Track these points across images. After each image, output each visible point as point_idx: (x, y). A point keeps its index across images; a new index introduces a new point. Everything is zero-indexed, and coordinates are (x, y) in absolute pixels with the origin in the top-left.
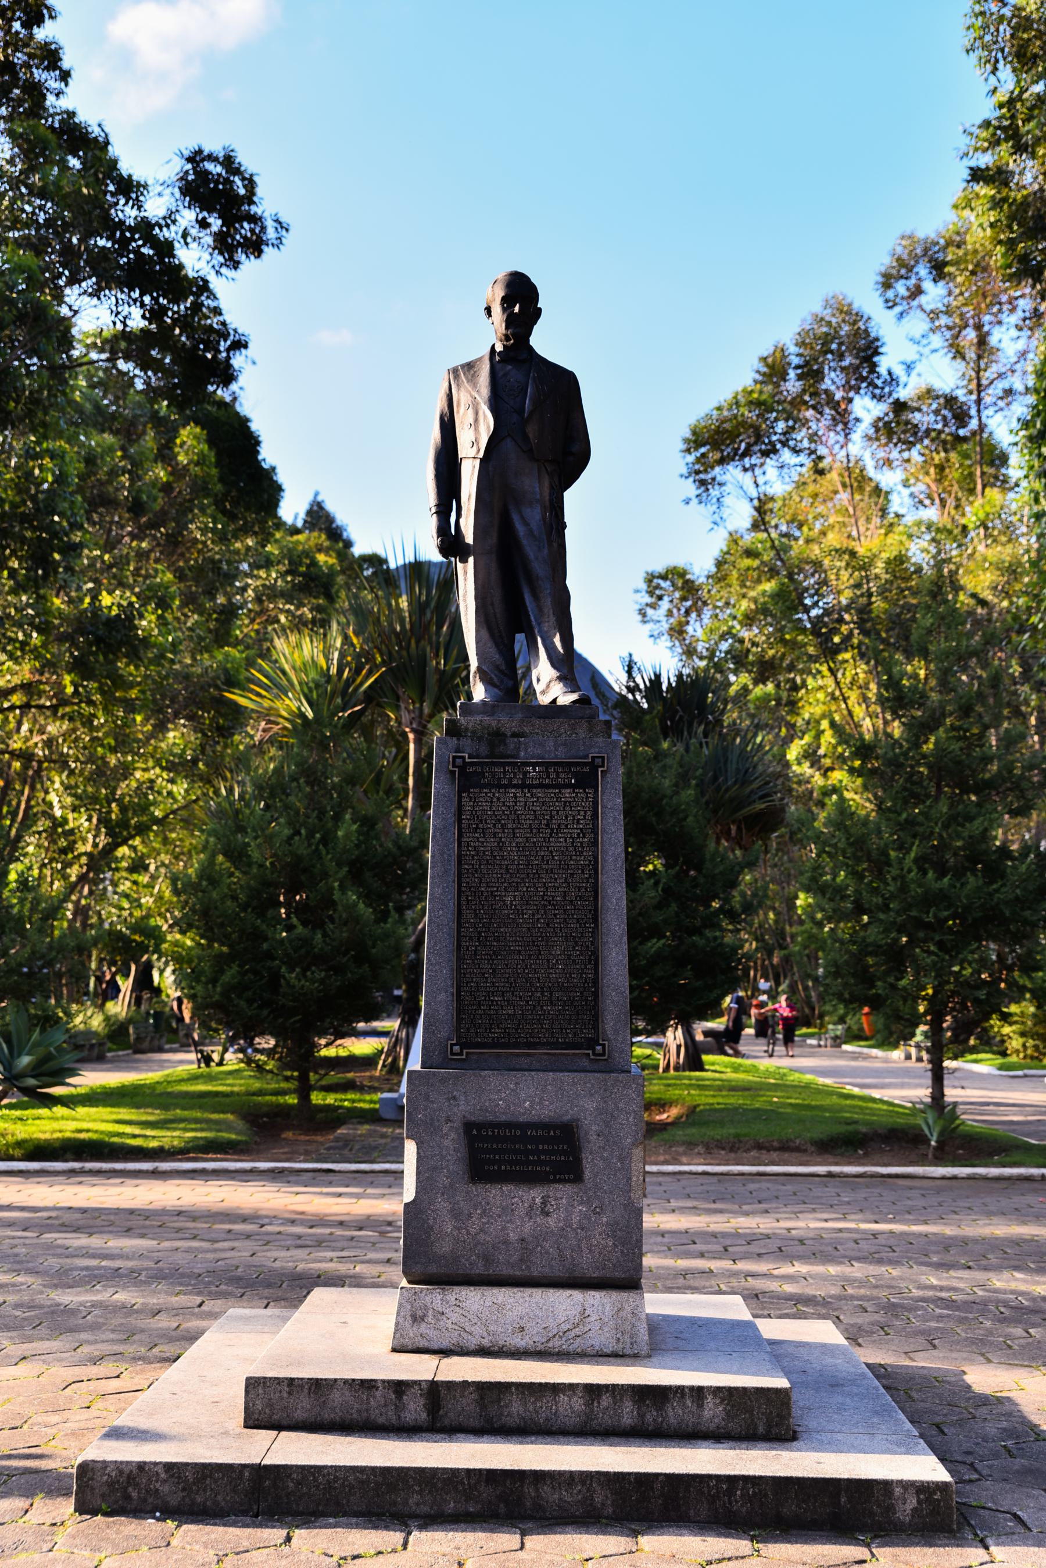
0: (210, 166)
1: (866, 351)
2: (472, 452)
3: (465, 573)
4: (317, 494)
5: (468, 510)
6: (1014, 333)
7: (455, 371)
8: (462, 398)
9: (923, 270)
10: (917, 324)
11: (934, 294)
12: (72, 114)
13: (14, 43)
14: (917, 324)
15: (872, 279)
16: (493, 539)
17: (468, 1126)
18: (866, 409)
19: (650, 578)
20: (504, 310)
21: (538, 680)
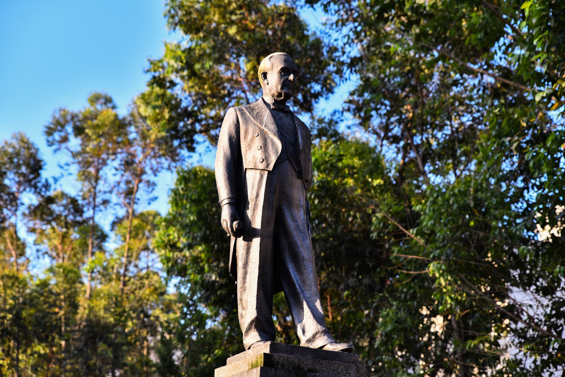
1: (36, 166)
6: (114, 171)
9: (69, 129)
10: (64, 157)
11: (75, 143)
14: (64, 157)
15: (42, 129)
16: (271, 228)
21: (304, 332)
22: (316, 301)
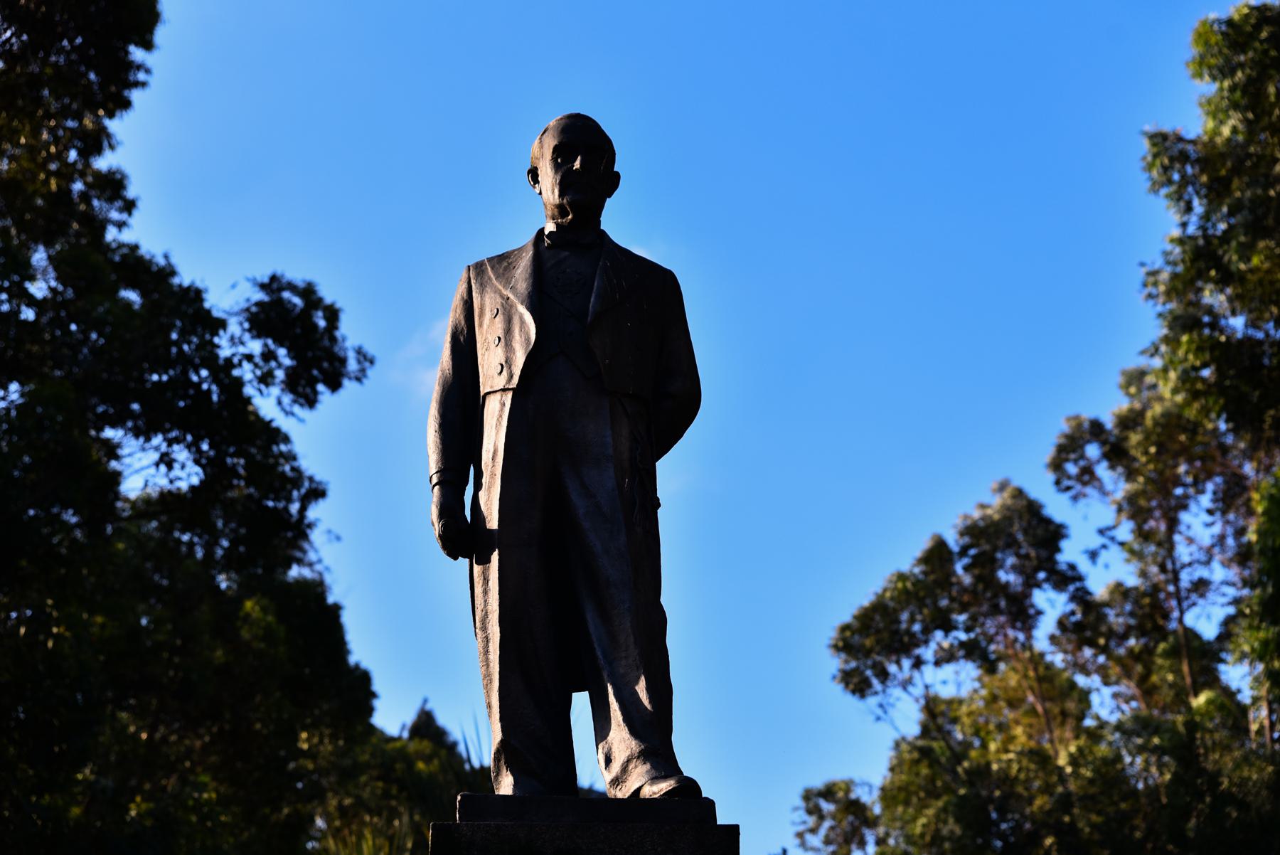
0: (286, 295)
1: (1052, 534)
2: (500, 382)
3: (486, 580)
4: (425, 701)
5: (493, 475)
7: (479, 268)
8: (487, 303)
9: (1093, 451)
12: (134, 248)
13: (67, 173)
18: (1051, 605)
19: (808, 796)
20: (557, 167)
22: (637, 682)
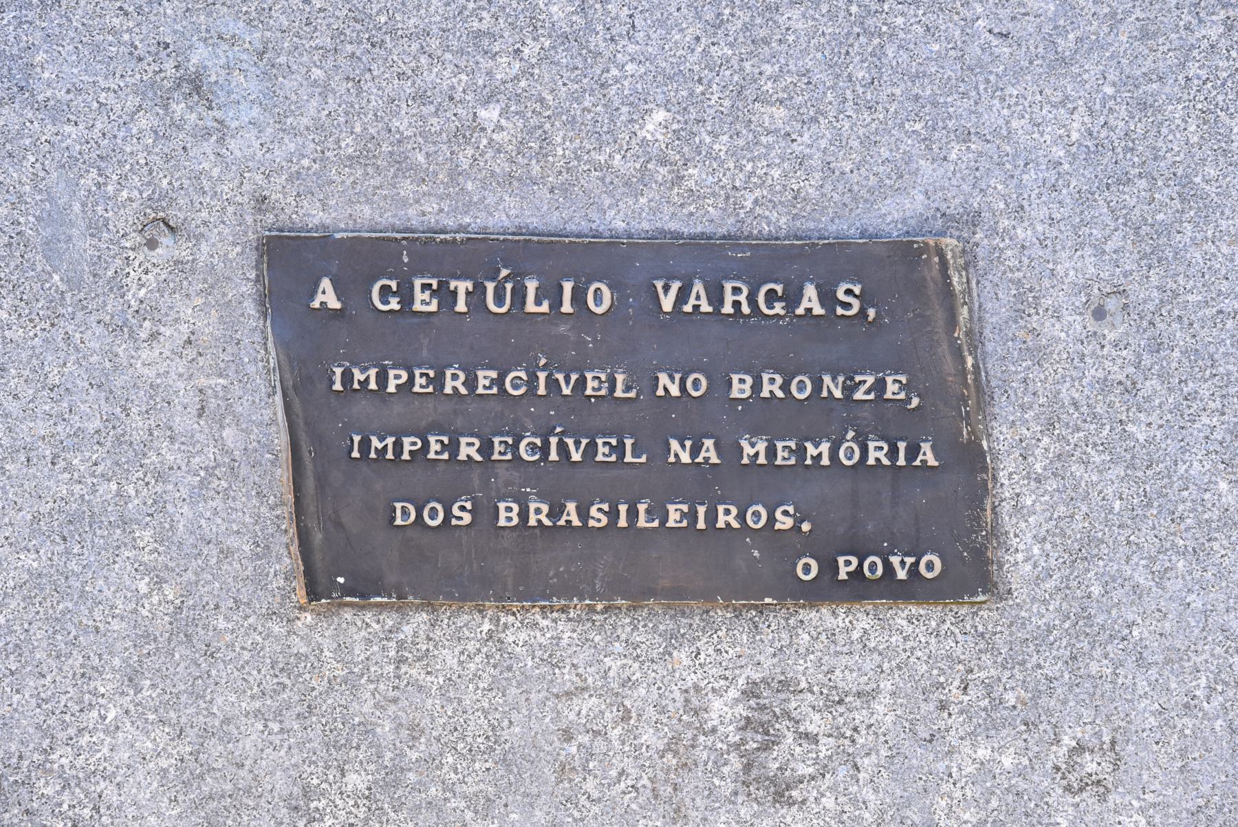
17: (289, 259)
